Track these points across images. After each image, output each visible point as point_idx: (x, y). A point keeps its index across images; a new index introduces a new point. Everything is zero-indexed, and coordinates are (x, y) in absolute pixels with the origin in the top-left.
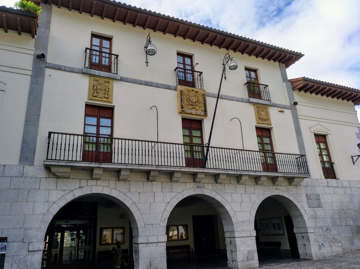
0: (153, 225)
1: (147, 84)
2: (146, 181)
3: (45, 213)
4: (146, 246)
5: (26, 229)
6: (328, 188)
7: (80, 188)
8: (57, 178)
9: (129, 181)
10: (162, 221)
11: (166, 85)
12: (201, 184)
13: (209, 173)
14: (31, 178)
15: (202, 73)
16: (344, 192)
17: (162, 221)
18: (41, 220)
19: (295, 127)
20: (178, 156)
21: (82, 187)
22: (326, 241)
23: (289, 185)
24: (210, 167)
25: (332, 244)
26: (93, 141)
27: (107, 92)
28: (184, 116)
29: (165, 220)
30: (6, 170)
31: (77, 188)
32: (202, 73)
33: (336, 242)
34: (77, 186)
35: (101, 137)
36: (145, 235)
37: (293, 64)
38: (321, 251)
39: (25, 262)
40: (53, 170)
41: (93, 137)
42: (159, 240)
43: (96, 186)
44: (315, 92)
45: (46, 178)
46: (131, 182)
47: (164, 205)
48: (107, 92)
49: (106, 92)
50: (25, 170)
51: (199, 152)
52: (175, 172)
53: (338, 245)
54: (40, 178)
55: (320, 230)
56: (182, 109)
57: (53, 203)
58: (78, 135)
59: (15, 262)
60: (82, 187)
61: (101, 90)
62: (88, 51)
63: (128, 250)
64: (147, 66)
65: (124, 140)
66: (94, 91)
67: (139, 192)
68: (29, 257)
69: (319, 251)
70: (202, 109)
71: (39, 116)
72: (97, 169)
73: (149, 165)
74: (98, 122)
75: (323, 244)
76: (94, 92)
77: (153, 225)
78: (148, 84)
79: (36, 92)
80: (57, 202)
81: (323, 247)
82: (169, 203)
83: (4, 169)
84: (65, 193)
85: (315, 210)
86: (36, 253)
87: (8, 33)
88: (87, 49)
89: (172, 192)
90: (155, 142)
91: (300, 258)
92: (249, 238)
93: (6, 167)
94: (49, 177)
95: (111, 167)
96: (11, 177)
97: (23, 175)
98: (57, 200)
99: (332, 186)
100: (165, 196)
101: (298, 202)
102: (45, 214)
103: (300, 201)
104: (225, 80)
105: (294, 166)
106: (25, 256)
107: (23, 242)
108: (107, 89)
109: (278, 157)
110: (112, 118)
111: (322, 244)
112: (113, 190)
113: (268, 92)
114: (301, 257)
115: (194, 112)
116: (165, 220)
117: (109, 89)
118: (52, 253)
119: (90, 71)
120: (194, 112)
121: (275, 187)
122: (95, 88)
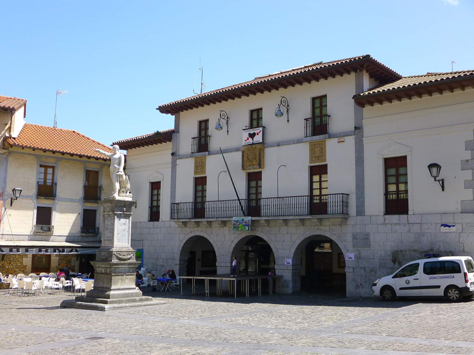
0: (224, 255)
5: (173, 253)
6: (384, 226)
7: (191, 232)
10: (228, 253)
12: (254, 227)
16: (408, 229)
22: (366, 282)
24: (332, 212)
26: (403, 198)
29: (230, 253)
34: (189, 232)
35: (401, 194)
37: (165, 114)
38: (357, 291)
41: (403, 193)
47: (230, 243)
51: (318, 199)
55: (363, 271)
58: (305, 196)
63: (39, 249)
65: (294, 197)
66: (313, 156)
69: (355, 290)
73: (301, 215)
74: (397, 171)
75: (362, 284)
77: (224, 255)
88: (306, 120)
89: (235, 234)
90: (276, 198)
92: (287, 271)
99: (390, 223)
101: (341, 241)
103: (342, 241)
104: (288, 123)
105: (285, 204)
109: (263, 202)
111: (361, 284)
113: (193, 145)
116: (230, 253)
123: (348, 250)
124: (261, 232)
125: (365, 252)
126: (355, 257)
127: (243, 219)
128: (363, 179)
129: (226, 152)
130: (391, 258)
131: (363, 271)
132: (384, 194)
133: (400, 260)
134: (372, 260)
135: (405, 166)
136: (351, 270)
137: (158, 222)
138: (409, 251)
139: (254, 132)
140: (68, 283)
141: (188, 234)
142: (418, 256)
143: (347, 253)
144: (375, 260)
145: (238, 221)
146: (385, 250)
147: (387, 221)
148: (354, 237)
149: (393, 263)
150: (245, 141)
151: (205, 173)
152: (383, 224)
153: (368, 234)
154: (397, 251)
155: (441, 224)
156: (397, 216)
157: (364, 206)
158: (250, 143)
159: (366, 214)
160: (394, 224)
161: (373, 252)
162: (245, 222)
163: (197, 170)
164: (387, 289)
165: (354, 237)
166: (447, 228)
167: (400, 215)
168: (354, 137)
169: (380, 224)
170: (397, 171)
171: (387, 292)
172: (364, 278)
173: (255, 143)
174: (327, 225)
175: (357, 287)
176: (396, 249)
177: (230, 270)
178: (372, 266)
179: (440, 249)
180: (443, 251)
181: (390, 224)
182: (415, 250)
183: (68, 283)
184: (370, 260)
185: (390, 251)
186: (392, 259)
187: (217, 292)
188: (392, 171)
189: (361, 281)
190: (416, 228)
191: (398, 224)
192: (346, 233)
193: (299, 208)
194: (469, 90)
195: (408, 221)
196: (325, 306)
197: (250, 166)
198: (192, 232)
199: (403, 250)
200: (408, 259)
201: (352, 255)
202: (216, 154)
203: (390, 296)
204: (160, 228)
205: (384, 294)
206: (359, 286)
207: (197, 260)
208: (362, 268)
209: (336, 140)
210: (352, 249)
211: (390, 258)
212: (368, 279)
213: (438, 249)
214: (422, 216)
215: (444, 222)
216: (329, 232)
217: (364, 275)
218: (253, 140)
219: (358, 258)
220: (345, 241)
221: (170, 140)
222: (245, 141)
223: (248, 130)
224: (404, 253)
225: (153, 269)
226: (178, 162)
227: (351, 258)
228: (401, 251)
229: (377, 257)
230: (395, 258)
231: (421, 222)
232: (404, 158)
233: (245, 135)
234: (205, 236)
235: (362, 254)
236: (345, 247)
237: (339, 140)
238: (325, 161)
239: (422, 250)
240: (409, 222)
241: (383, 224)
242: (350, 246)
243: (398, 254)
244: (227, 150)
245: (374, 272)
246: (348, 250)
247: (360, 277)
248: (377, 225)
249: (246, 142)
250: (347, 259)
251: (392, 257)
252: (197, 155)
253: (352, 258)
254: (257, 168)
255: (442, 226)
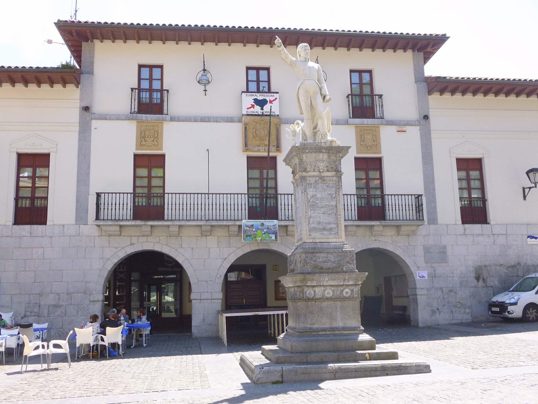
1: (204, 119)
2: (199, 235)
3: (101, 268)
4: (199, 303)
5: (86, 282)
6: (464, 237)
8: (109, 236)
9: (181, 236)
11: (227, 118)
13: (46, 217)
14: (87, 237)
15: (382, 95)
16: (493, 241)
17: (217, 278)
18: (98, 276)
19: (423, 153)
20: (350, 208)
21: (133, 244)
22: (445, 305)
23: (397, 235)
25: (453, 310)
27: (156, 138)
28: (248, 155)
29: (220, 277)
30: (65, 230)
31: (129, 245)
32: (382, 95)
33: (461, 308)
34: (129, 243)
36: (198, 291)
38: (434, 318)
39: (89, 310)
40: (103, 228)
42: (214, 297)
43: (147, 243)
44: (524, 93)
45: (99, 236)
46: (183, 237)
48: (156, 138)
49: (155, 139)
50: (80, 229)
52: (231, 226)
53: (465, 312)
54: (94, 237)
55: (439, 291)
56: (246, 147)
57: (107, 260)
59: (80, 309)
60: (133, 244)
61: (149, 137)
62: (350, 96)
64: (205, 95)
65: (353, 196)
67: (193, 248)
68: (91, 306)
70: (274, 144)
71: (89, 174)
72: (144, 226)
74: (150, 173)
75: (439, 308)
76: (142, 141)
78: (205, 119)
79: (85, 149)
80: (111, 258)
81: (438, 313)
82: (227, 259)
83: (64, 229)
84: (117, 250)
85: (434, 267)
86: (96, 302)
87: (41, 88)
88: (132, 89)
89: (231, 247)
91: (410, 324)
93: (65, 227)
94: (102, 235)
95: (158, 224)
96: (70, 236)
97: (79, 234)
98: (111, 257)
100: (221, 252)
101: (408, 256)
102: (101, 269)
106: (88, 306)
107: (85, 293)
108: (156, 135)
109: (389, 200)
110: (163, 167)
111: (438, 309)
112: (164, 246)
114: (412, 324)
115: (262, 149)
117: (157, 134)
118: (145, 306)
119: (136, 116)
120: (262, 149)
121: (373, 238)
122: (143, 135)
123: (418, 267)
124: (281, 244)
125: (441, 269)
126: (428, 276)
127: (262, 223)
128: (433, 180)
129: (207, 120)
130: (474, 274)
131: (439, 292)
132: (486, 200)
133: (485, 277)
134: (450, 278)
135: (47, 166)
136: (425, 292)
137: (45, 226)
138: (494, 265)
139: (265, 98)
140: (37, 348)
141: (124, 248)
142: (505, 271)
143: (417, 271)
144: (454, 278)
145: (253, 225)
146: (466, 265)
147: (468, 232)
148: (427, 251)
149: (476, 281)
150: (248, 109)
151: (161, 149)
152: (462, 235)
153: (445, 247)
154: (480, 266)
155: (527, 236)
156: (480, 225)
157: (436, 212)
158: (256, 114)
159: (439, 222)
160: (476, 235)
161: (452, 268)
162: (268, 228)
163: (144, 143)
164: (531, 308)
165: (427, 251)
166: (534, 239)
167: (482, 225)
168: (418, 128)
169: (459, 235)
170: (150, 173)
171: (531, 311)
172: (441, 301)
173: (266, 114)
174: (389, 234)
175: (433, 312)
176: (480, 264)
177: (221, 304)
178: (451, 286)
179: (528, 262)
180: (530, 265)
181: (472, 235)
182: (501, 265)
183: (37, 348)
184: (448, 278)
185: (473, 266)
186: (475, 276)
187: (19, 354)
188: (143, 172)
189: (437, 305)
190: (501, 240)
191: (482, 234)
192: (416, 246)
193: (399, 210)
194: (533, 98)
195: (492, 232)
196: (128, 358)
197: (259, 146)
198: (134, 244)
199: (488, 265)
200: (494, 275)
201: (425, 274)
202: (183, 121)
203: (536, 315)
204: (51, 237)
205: (528, 314)
206: (435, 312)
207: (536, 276)
208: (438, 288)
209: (394, 128)
210: (425, 265)
211: (473, 275)
212: (446, 301)
213: (526, 263)
214: (507, 227)
215: (530, 234)
216: (392, 244)
217: (441, 297)
218: (262, 109)
219: (433, 276)
220: (415, 256)
221: (77, 83)
222: (248, 109)
223: (253, 94)
224: (489, 268)
225: (28, 313)
226: (95, 123)
227: (423, 277)
228: (485, 266)
229: (457, 274)
230: (479, 275)
231: (507, 233)
232: (47, 156)
233: (248, 100)
234: (166, 250)
235: (437, 272)
236: (415, 263)
237: (400, 129)
238: (380, 153)
239: (509, 265)
240: (494, 233)
241: (462, 235)
242: (421, 261)
243: (482, 270)
244: (208, 117)
245: (454, 292)
246: (419, 267)
247: (436, 300)
248: (456, 236)
249: (249, 110)
250: (418, 278)
251: (476, 274)
252: (146, 117)
253: (425, 277)
254: (273, 151)
255: (528, 237)
